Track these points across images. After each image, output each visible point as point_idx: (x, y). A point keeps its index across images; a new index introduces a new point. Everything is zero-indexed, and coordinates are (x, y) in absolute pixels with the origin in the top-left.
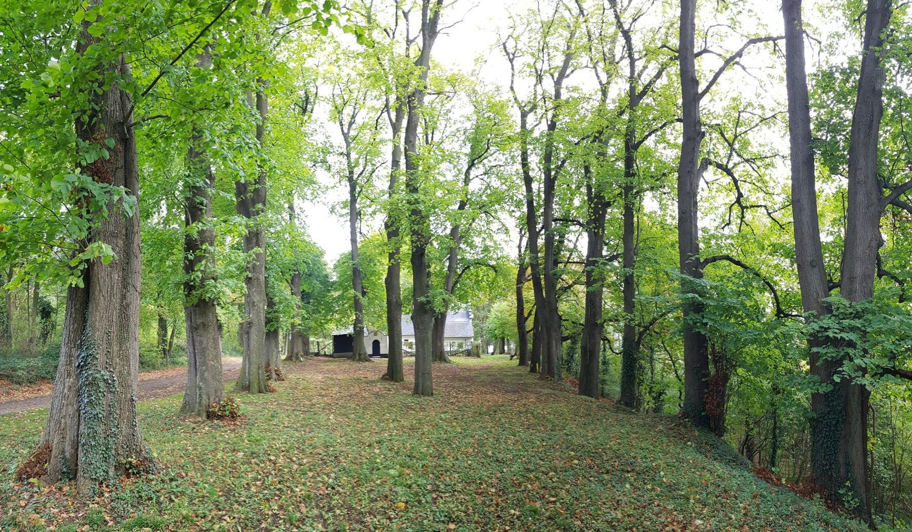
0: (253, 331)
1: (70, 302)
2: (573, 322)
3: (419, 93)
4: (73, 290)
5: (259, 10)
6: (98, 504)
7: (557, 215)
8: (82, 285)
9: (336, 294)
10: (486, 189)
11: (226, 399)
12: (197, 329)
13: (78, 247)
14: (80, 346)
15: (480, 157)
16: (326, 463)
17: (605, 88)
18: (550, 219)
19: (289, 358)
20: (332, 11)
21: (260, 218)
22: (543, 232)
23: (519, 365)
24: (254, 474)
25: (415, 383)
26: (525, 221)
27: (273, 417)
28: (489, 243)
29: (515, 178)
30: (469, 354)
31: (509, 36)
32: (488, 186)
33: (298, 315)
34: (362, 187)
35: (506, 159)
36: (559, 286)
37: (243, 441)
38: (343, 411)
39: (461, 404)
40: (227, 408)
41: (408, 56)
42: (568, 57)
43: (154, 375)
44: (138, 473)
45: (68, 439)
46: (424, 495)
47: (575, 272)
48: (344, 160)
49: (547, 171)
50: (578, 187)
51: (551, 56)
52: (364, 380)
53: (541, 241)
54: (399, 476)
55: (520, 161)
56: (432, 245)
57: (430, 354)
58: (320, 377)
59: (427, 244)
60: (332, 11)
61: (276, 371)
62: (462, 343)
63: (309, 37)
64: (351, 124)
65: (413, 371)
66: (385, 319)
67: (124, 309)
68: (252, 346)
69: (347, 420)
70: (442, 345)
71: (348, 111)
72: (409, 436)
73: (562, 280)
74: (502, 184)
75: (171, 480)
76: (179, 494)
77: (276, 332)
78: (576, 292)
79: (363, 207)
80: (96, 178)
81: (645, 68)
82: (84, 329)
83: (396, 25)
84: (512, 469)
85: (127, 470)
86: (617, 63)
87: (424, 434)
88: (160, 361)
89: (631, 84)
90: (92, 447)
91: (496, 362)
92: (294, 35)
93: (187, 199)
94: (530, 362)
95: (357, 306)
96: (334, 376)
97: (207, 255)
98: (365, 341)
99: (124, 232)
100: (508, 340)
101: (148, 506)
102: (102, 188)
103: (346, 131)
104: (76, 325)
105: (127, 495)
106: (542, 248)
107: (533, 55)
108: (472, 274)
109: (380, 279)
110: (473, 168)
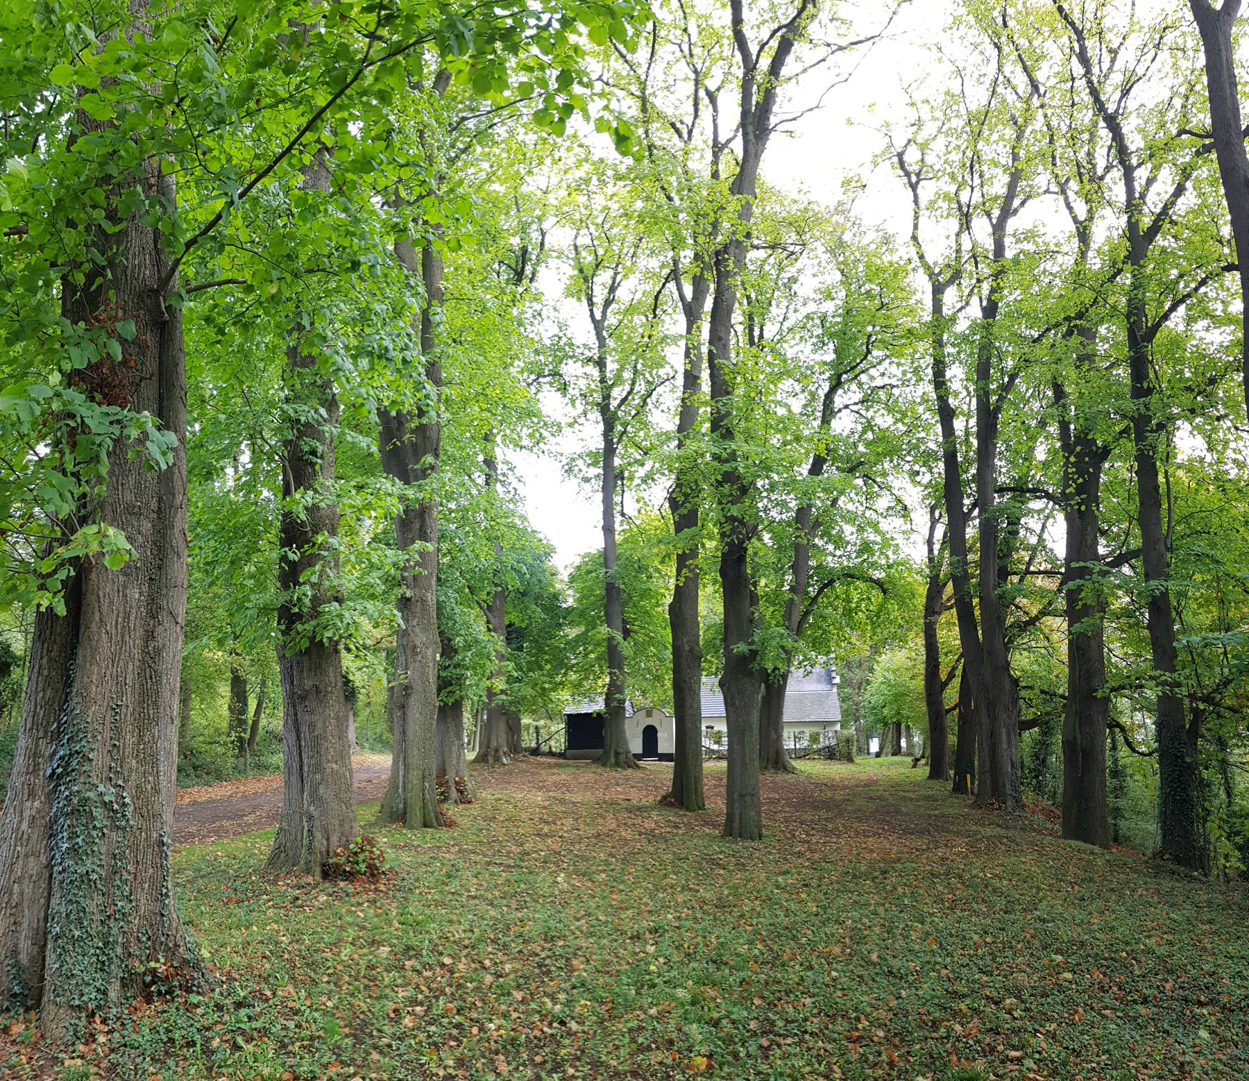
0: (414, 703)
1: (39, 645)
2: (1043, 692)
3: (736, 247)
4: (46, 619)
5: (428, 84)
6: (82, 1057)
7: (1002, 479)
8: (61, 610)
9: (572, 632)
10: (864, 432)
11: (359, 840)
12: (303, 698)
13: (59, 534)
14: (57, 736)
15: (853, 368)
16: (548, 973)
17: (1085, 228)
18: (990, 488)
19: (482, 758)
20: (577, 89)
21: (432, 482)
22: (976, 512)
23: (931, 777)
24: (409, 992)
25: (727, 814)
26: (942, 492)
27: (449, 876)
28: (872, 536)
29: (921, 409)
30: (830, 754)
31: (909, 141)
32: (869, 426)
33: (500, 672)
34: (625, 425)
35: (904, 373)
36: (1010, 620)
37: (391, 925)
38: (582, 866)
39: (817, 856)
40: (361, 857)
41: (715, 175)
42: (1015, 177)
43: (218, 791)
44: (169, 992)
45: (25, 925)
46: (744, 1043)
47: (1042, 592)
48: (594, 372)
49: (983, 396)
50: (1043, 424)
51: (986, 177)
52: (624, 804)
53: (971, 531)
54: (693, 1003)
55: (931, 376)
56: (760, 539)
57: (756, 756)
58: (539, 797)
59: (749, 539)
60: (577, 89)
61: (457, 783)
62: (818, 734)
63: (531, 138)
64: (608, 303)
65: (723, 790)
66: (669, 684)
67: (151, 658)
68: (410, 733)
69: (589, 884)
70: (779, 737)
71: (603, 278)
72: (715, 920)
73: (1017, 607)
74: (897, 421)
75: (239, 1005)
76: (255, 1034)
77: (457, 707)
78: (1047, 631)
79: (629, 464)
80: (98, 397)
81: (1150, 181)
82: (66, 701)
83: (696, 116)
84: (921, 993)
85: (148, 986)
86: (1102, 178)
87: (742, 916)
88: (231, 762)
89: (1130, 218)
90: (74, 940)
91: (884, 771)
92: (501, 131)
93: (286, 443)
94: (952, 772)
95: (613, 658)
96: (568, 796)
97: (325, 553)
98: (626, 727)
99: (154, 505)
100: (908, 727)
101: (185, 1059)
102: (108, 414)
103: (598, 316)
104: (49, 691)
105: (144, 1037)
106: (974, 544)
107: (953, 177)
108: (837, 597)
109: (658, 605)
110: (840, 392)
